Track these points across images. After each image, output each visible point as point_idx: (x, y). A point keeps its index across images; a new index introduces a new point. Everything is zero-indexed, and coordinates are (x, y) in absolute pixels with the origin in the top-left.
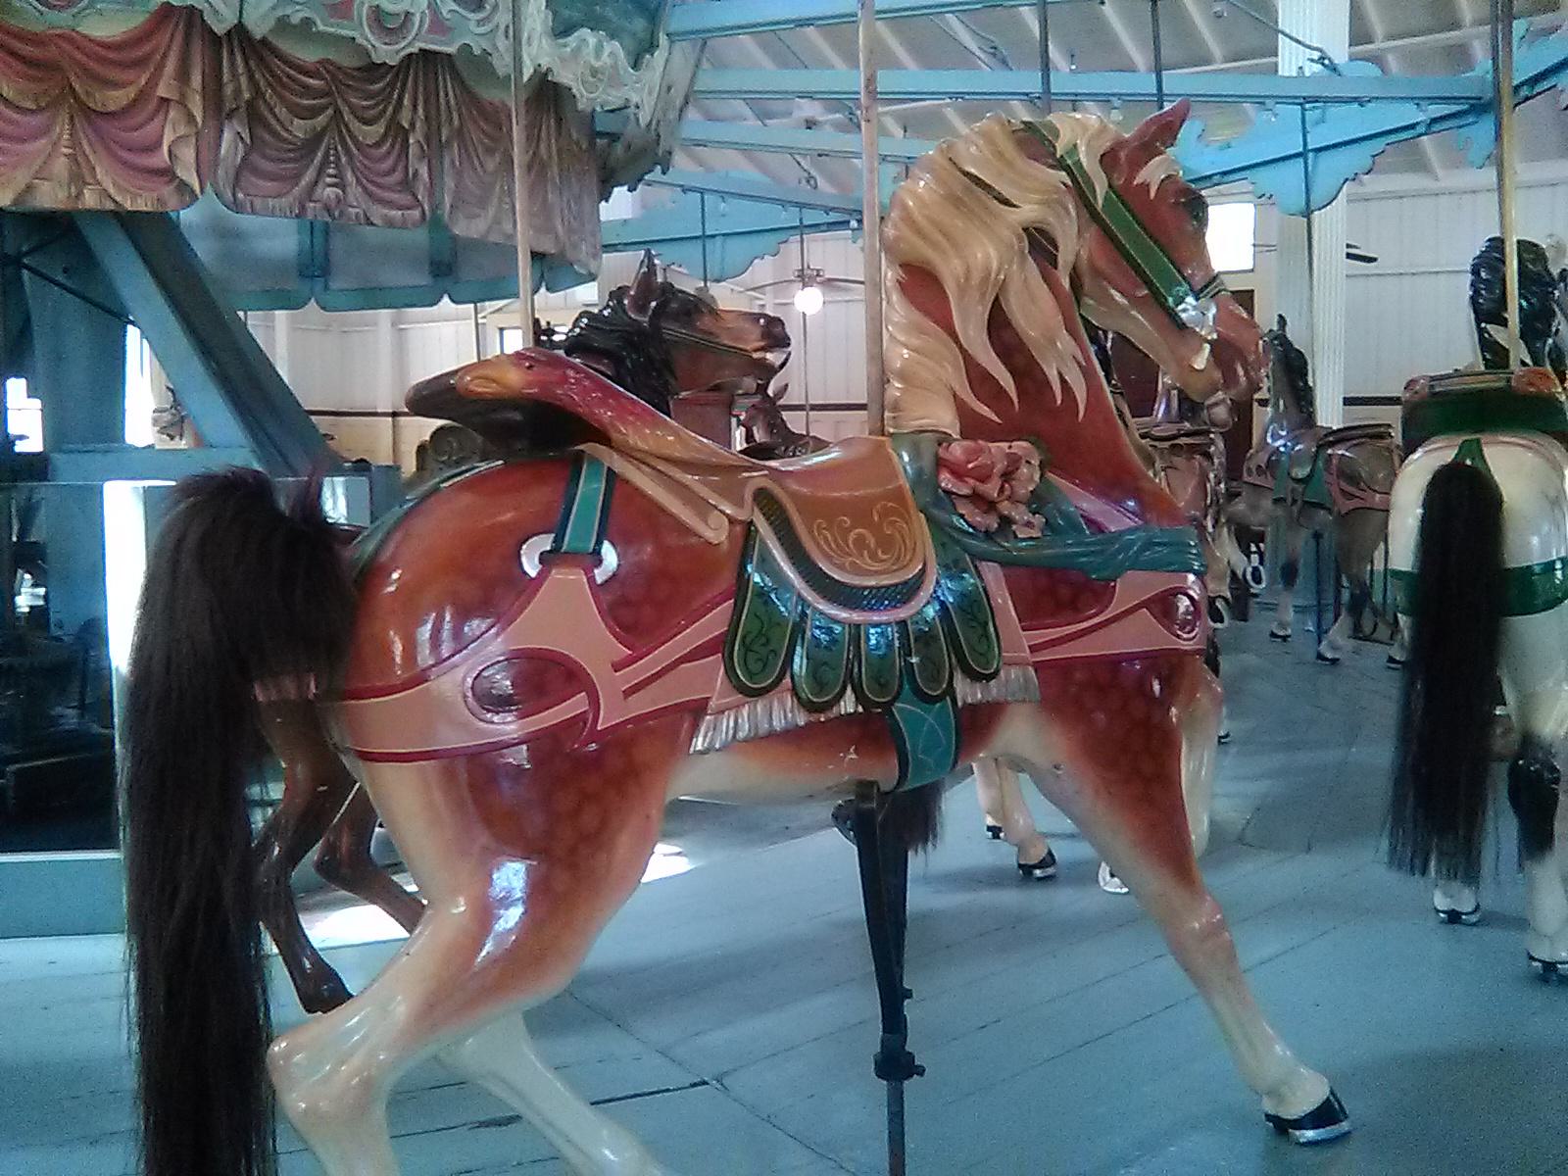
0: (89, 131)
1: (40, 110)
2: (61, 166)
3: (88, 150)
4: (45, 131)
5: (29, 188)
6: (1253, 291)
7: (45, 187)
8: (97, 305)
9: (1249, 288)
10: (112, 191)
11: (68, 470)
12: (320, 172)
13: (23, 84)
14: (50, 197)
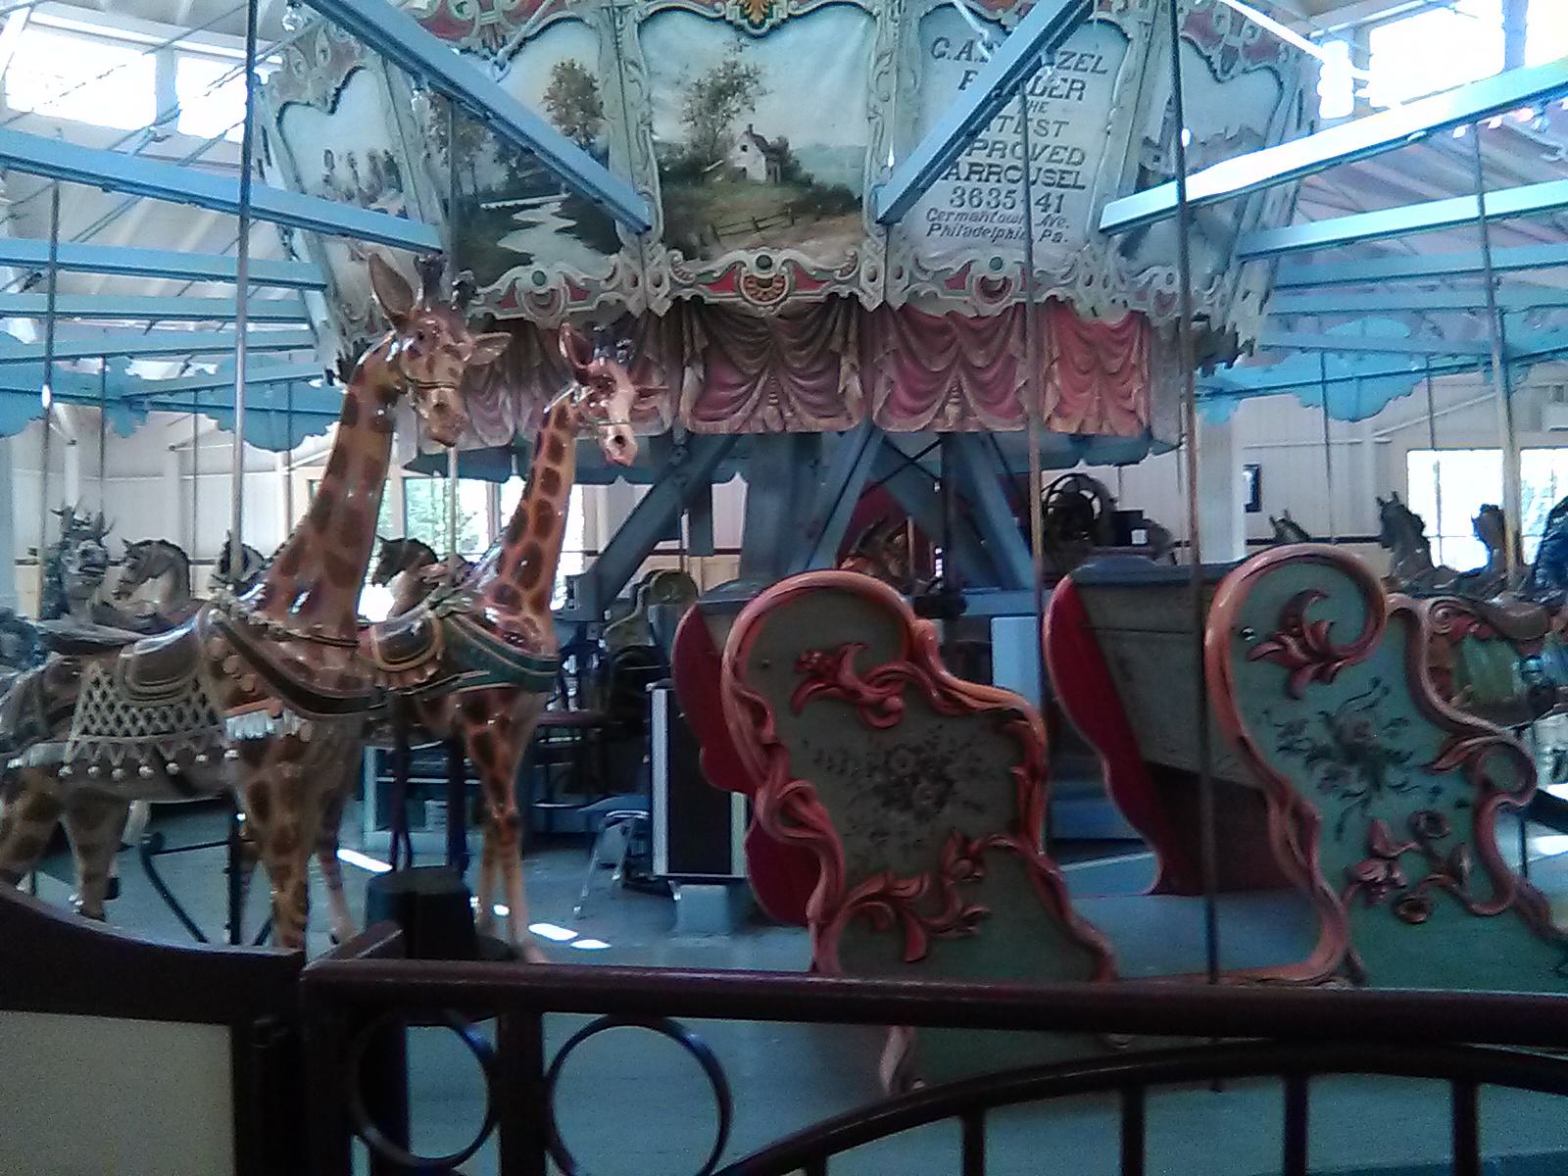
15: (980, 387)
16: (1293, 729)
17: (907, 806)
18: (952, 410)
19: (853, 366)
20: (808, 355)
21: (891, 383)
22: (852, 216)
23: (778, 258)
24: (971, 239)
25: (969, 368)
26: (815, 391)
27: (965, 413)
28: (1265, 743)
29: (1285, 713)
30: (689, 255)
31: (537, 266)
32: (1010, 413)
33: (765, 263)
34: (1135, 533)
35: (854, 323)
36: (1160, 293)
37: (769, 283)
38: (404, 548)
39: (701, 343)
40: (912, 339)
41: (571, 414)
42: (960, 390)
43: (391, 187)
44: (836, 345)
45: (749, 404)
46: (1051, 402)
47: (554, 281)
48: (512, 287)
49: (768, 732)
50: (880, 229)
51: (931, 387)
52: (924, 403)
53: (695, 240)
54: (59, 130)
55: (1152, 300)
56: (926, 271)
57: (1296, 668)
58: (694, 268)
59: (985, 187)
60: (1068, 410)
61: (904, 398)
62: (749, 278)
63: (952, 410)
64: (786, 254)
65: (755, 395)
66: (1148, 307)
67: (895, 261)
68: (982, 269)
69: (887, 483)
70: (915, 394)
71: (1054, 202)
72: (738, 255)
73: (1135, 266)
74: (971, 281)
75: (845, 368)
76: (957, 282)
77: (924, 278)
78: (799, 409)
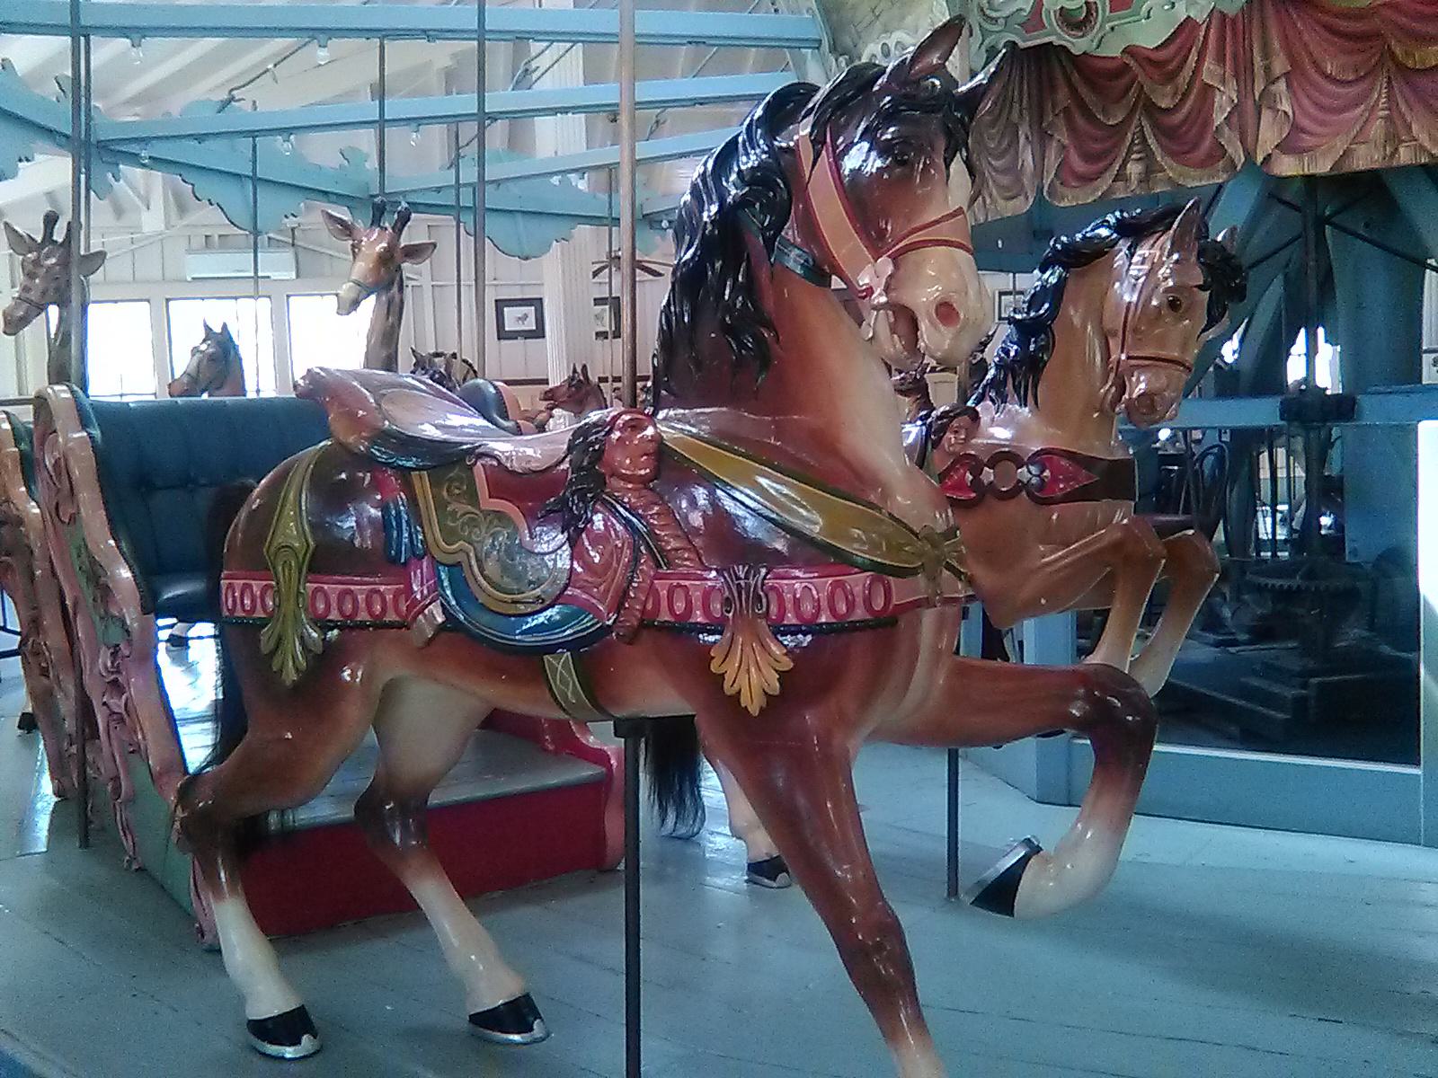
0: (1406, 90)
1: (1359, 80)
2: (1377, 129)
3: (1403, 108)
4: (1363, 97)
5: (1347, 153)
6: (496, 301)
7: (1361, 150)
8: (1396, 253)
9: (538, 296)
10: (1427, 144)
11: (1373, 409)
12: (1130, 152)
13: (1343, 59)
14: (1366, 158)
15: (1168, 134)
18: (1134, 169)
20: (998, 132)
25: (1151, 109)
27: (1150, 170)
32: (1204, 164)
40: (1084, 91)
42: (1144, 140)
44: (1015, 116)
51: (1107, 145)
52: (1101, 165)
54: (1393, 601)
56: (996, 20)
60: (1308, 141)
61: (1079, 165)
63: (1134, 169)
70: (1088, 157)
77: (995, 28)
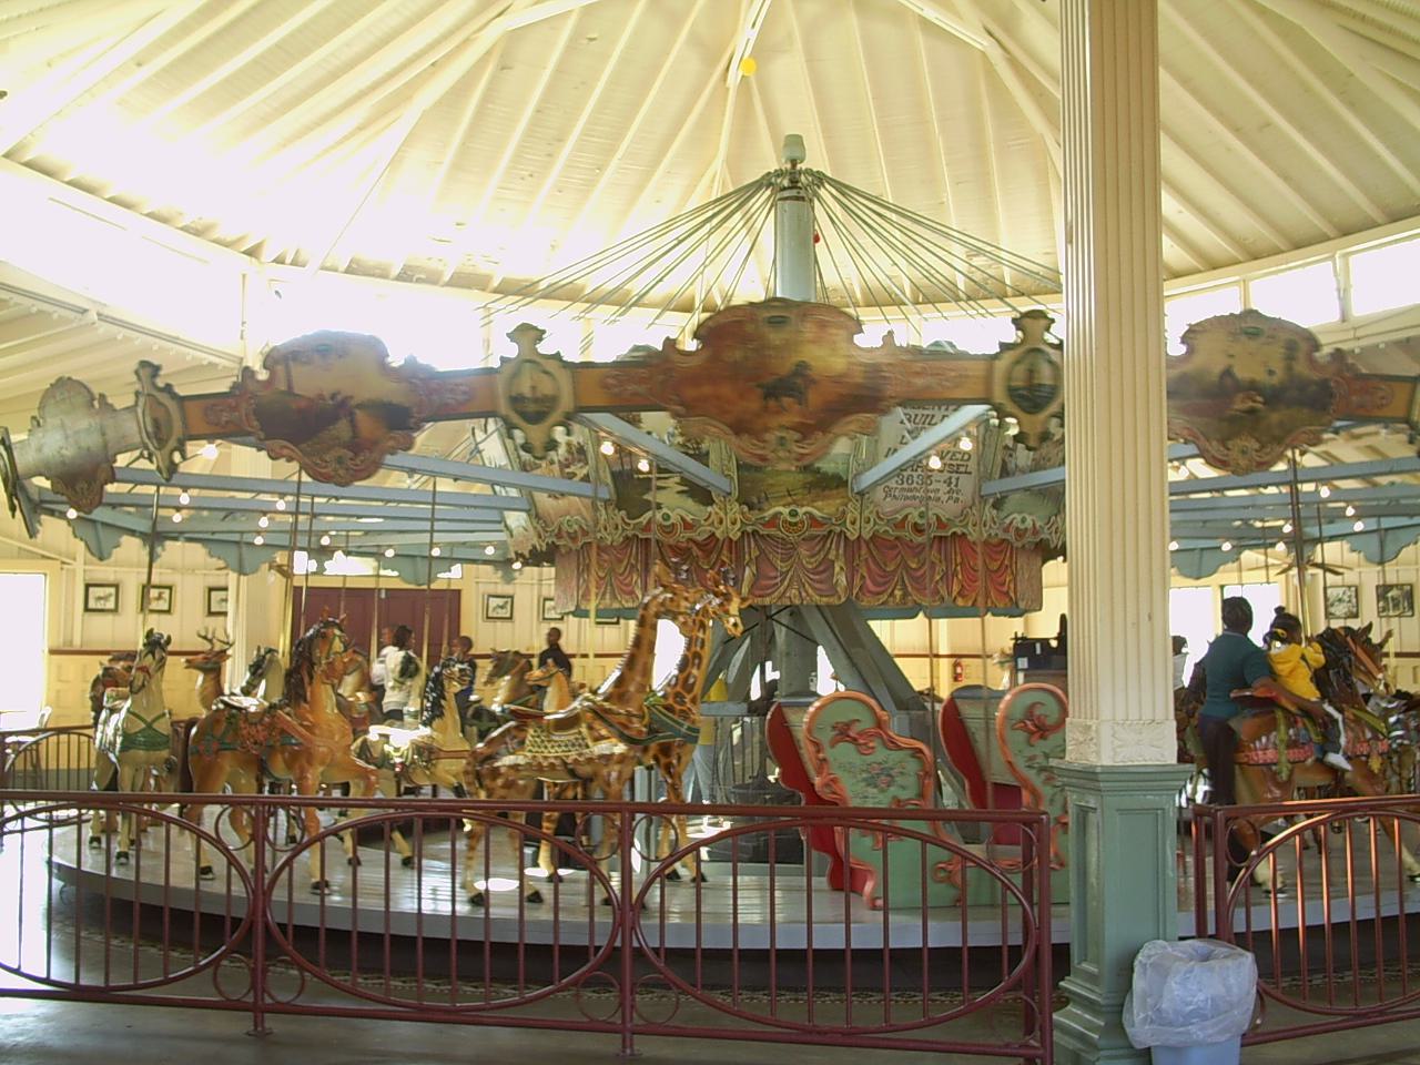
15: (915, 580)
16: (1032, 758)
17: (876, 787)
18: (898, 593)
19: (842, 568)
21: (863, 577)
22: (841, 490)
23: (801, 511)
24: (908, 502)
25: (907, 567)
26: (821, 582)
28: (1020, 764)
29: (1029, 752)
30: (751, 508)
31: (665, 510)
33: (793, 514)
34: (1025, 660)
35: (842, 544)
36: (1017, 528)
37: (796, 524)
38: (510, 657)
39: (755, 553)
41: (710, 610)
43: (580, 461)
44: (831, 556)
45: (782, 589)
46: (956, 588)
47: (674, 518)
48: (649, 522)
49: (821, 755)
50: (858, 497)
53: (755, 500)
55: (1012, 531)
57: (1032, 733)
58: (754, 515)
59: (915, 474)
61: (872, 587)
62: (785, 521)
63: (898, 593)
64: (805, 509)
65: (786, 583)
66: (1011, 536)
67: (866, 513)
68: (914, 517)
69: (960, 923)
71: (953, 480)
72: (781, 509)
73: (1002, 515)
74: (909, 526)
75: (837, 569)
76: (900, 525)
78: (810, 591)
